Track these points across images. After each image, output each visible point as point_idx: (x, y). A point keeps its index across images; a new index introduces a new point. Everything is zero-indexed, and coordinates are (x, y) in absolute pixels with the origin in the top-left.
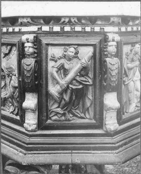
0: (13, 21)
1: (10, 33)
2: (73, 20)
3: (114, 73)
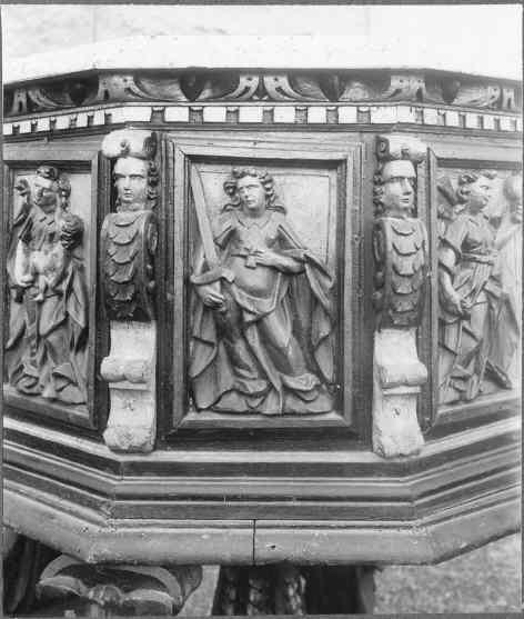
0: (79, 88)
2: (270, 82)
3: (404, 287)
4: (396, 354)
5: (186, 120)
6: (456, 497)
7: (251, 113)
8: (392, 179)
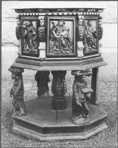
2: (63, 10)
8: (80, 22)
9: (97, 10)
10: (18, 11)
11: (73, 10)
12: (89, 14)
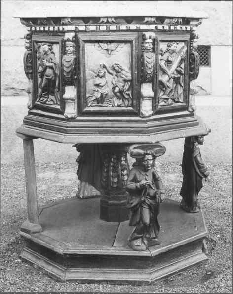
1: (42, 31)
2: (110, 20)
4: (147, 90)
5: (105, 29)
6: (100, 132)
7: (103, 28)
8: (146, 43)
9: (186, 21)
10: (26, 21)
11: (132, 21)
12: (170, 28)
